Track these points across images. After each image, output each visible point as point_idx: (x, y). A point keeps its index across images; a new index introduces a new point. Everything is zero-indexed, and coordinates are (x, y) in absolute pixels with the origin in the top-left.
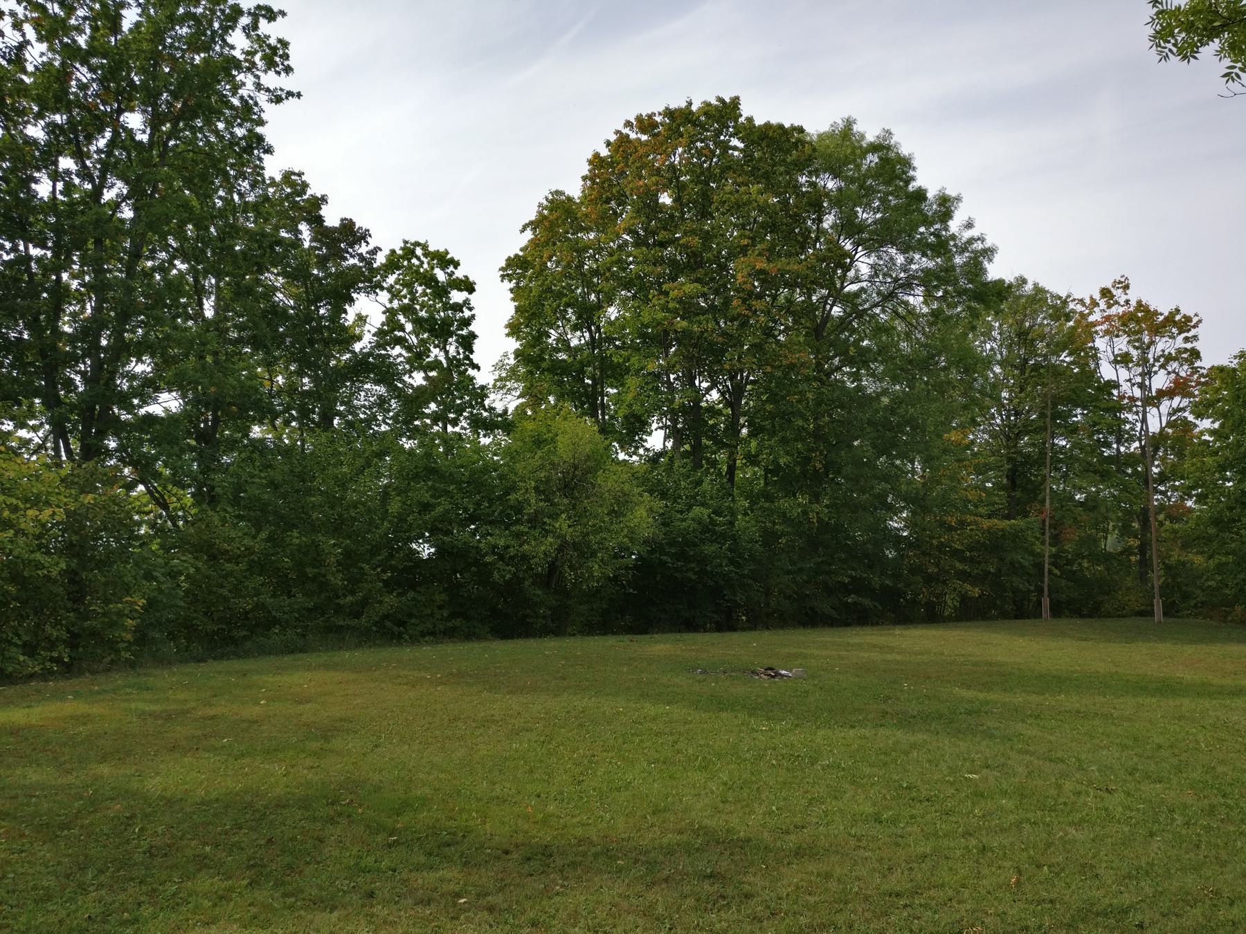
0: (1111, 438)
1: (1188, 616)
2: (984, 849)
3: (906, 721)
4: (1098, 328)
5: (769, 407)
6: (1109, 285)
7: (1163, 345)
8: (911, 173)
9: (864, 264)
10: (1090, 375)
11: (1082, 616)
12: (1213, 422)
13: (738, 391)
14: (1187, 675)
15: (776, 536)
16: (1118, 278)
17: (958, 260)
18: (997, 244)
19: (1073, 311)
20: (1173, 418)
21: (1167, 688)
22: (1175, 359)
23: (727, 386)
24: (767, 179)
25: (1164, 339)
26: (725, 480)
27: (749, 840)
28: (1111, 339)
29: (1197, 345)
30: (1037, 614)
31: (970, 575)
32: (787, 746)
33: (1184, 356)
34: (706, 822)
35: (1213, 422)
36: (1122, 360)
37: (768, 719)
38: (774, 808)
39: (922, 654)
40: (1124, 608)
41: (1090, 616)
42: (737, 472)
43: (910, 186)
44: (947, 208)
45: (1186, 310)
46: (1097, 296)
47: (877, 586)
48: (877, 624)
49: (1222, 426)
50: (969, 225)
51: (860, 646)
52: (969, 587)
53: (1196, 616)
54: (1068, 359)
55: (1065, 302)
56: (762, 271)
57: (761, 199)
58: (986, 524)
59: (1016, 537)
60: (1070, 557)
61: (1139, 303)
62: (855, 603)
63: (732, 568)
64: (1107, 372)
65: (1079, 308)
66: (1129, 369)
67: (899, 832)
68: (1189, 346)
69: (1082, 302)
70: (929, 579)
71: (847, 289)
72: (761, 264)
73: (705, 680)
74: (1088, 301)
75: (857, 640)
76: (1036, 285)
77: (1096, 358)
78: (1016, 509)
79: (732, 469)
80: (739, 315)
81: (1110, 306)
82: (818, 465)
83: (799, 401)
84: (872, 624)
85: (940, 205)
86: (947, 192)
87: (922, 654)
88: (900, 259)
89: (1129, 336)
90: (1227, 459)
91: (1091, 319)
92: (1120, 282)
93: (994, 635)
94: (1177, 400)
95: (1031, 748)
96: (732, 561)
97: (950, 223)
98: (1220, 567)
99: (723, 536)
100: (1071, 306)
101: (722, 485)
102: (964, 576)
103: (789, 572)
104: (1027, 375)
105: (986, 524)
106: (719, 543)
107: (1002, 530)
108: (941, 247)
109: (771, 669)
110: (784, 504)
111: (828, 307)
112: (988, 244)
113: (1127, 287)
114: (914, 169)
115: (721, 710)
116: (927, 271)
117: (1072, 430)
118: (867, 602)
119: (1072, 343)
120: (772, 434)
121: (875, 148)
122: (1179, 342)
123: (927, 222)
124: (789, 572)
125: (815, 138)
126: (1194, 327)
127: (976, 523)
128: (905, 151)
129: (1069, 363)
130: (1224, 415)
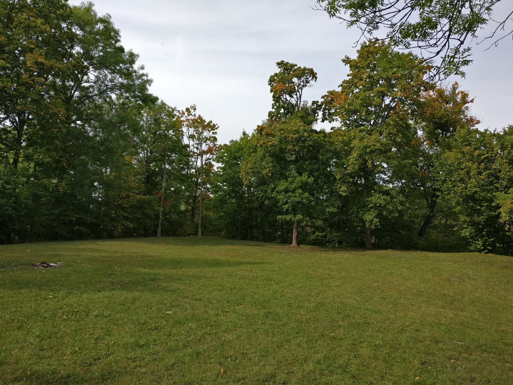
0: (185, 167)
1: (207, 235)
2: (198, 354)
3: (124, 286)
4: (184, 123)
5: (41, 132)
6: (189, 107)
7: (206, 134)
8: (119, 38)
9: (92, 75)
10: (179, 141)
11: (169, 236)
12: (222, 164)
13: (22, 122)
14: (222, 258)
15: (40, 197)
16: (192, 105)
17: (137, 82)
18: (153, 79)
19: (175, 115)
20: (207, 162)
21: (217, 263)
22: (209, 140)
23: (15, 119)
24: (46, 19)
25: (206, 132)
26: (12, 167)
27: (69, 376)
28: (188, 128)
29: (216, 136)
30: (154, 234)
31: (129, 218)
32: (68, 306)
33: (212, 139)
34: (35, 368)
35: (222, 164)
36: (192, 137)
37: (52, 291)
38: (77, 349)
39: (115, 252)
40: (185, 233)
41: (172, 236)
42: (19, 164)
43: (117, 44)
44: (133, 59)
45: (214, 122)
46: (184, 111)
47: (89, 222)
48: (87, 239)
49: (225, 166)
50: (142, 68)
51: (85, 250)
52: (129, 223)
53: (209, 235)
54: (172, 133)
55: (173, 110)
56: (42, 64)
57: (43, 27)
58: (138, 197)
59: (149, 203)
60: (167, 212)
61: (199, 116)
62: (77, 230)
63: (14, 212)
64: (186, 141)
65: (178, 114)
66: (193, 140)
67: (151, 351)
68: (214, 135)
69: (179, 111)
70: (112, 220)
71: (83, 85)
72: (41, 60)
73: (5, 271)
74: (181, 112)
75: (81, 247)
76: (162, 102)
77: (183, 135)
78: (148, 192)
79: (16, 162)
80: (27, 83)
81: (189, 115)
82: (65, 164)
83: (57, 132)
84: (84, 239)
85: (130, 56)
86: (133, 51)
87: (115, 252)
88: (109, 77)
89: (194, 128)
90: (226, 178)
91: (182, 119)
92: (193, 107)
93: (142, 244)
94: (208, 155)
95: (186, 295)
96: (14, 208)
97: (134, 65)
98: (220, 218)
99: (10, 196)
100: (175, 112)
101: (10, 169)
102: (126, 218)
103: (46, 215)
104: (156, 137)
105: (138, 197)
106: (7, 199)
107: (144, 200)
108: (128, 74)
109: (45, 263)
110: (45, 181)
111: (73, 91)
112: (149, 78)
113: (195, 109)
114: (120, 36)
115: (20, 288)
116: (122, 84)
117: (171, 163)
118: (83, 229)
119: (175, 127)
120: (41, 146)
121: (102, 21)
122: (211, 134)
123: (124, 62)
124: (46, 215)
125: (72, 7)
126: (217, 129)
127: (134, 196)
128: (116, 27)
129: (173, 135)
130: (226, 162)
